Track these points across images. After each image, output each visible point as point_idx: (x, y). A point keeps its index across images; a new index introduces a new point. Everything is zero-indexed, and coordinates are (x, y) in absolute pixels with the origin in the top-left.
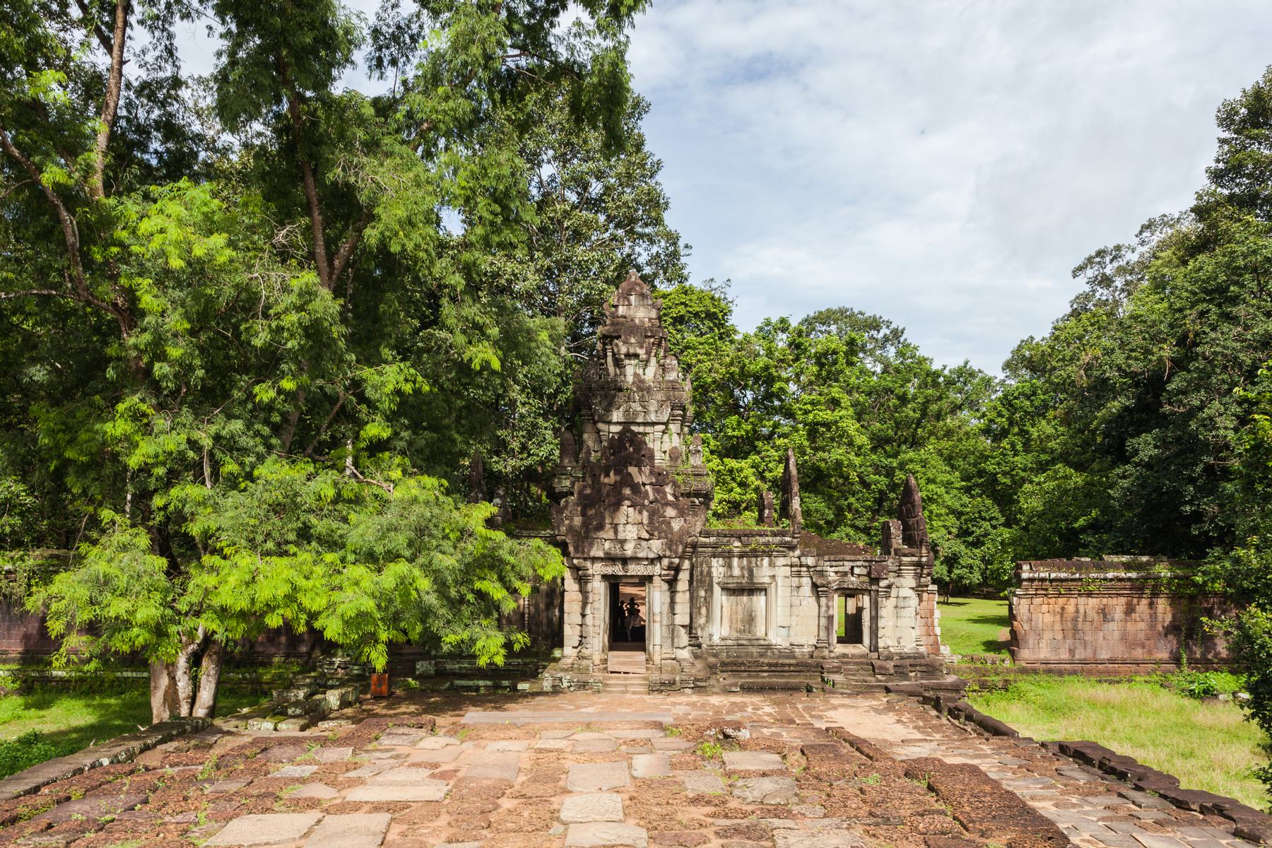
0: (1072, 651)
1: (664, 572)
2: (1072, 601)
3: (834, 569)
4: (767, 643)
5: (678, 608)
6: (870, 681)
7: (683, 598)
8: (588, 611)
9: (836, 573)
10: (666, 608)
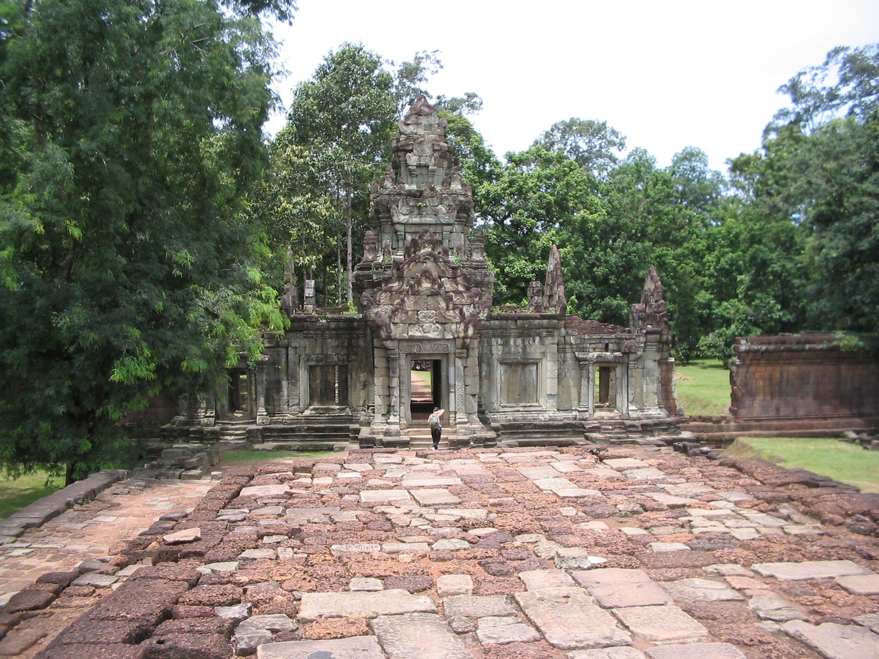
0: (778, 410)
1: (458, 351)
2: (778, 369)
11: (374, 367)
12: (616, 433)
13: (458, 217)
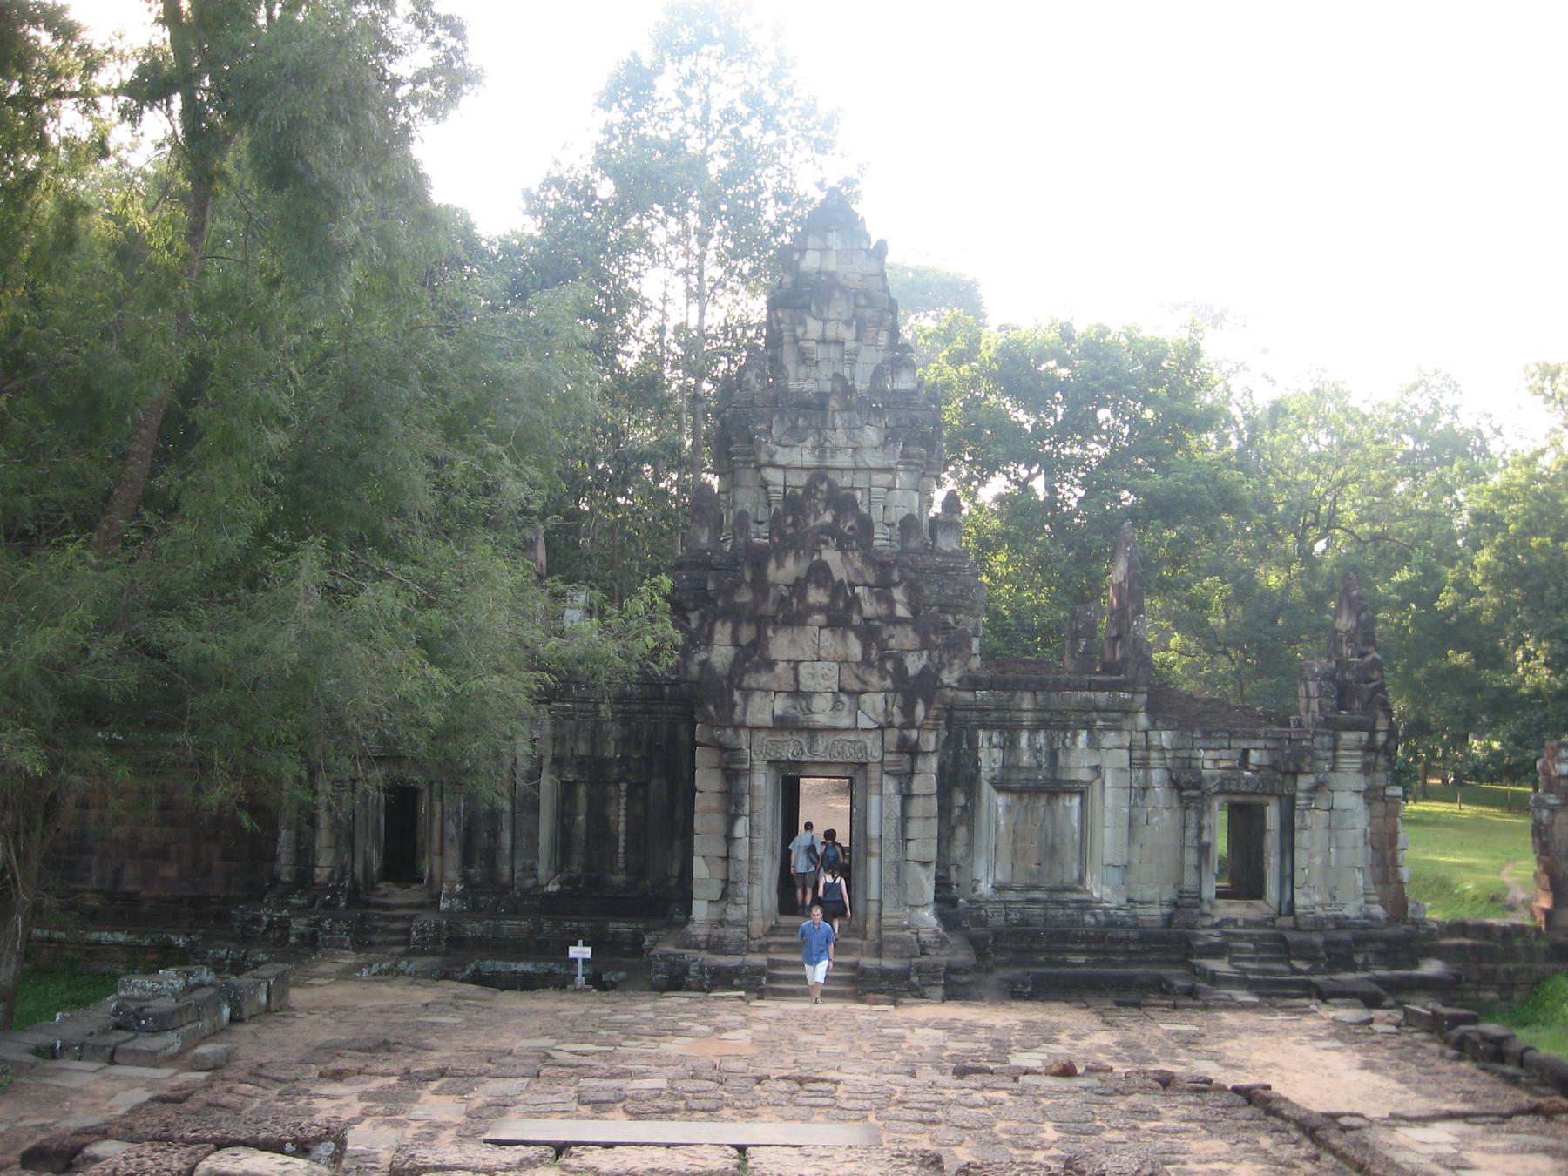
3: (1211, 754)
4: (1084, 896)
5: (914, 829)
6: (1281, 973)
7: (925, 807)
8: (741, 828)
9: (1215, 761)
10: (891, 828)
11: (695, 790)
12: (1262, 960)
13: (904, 454)
